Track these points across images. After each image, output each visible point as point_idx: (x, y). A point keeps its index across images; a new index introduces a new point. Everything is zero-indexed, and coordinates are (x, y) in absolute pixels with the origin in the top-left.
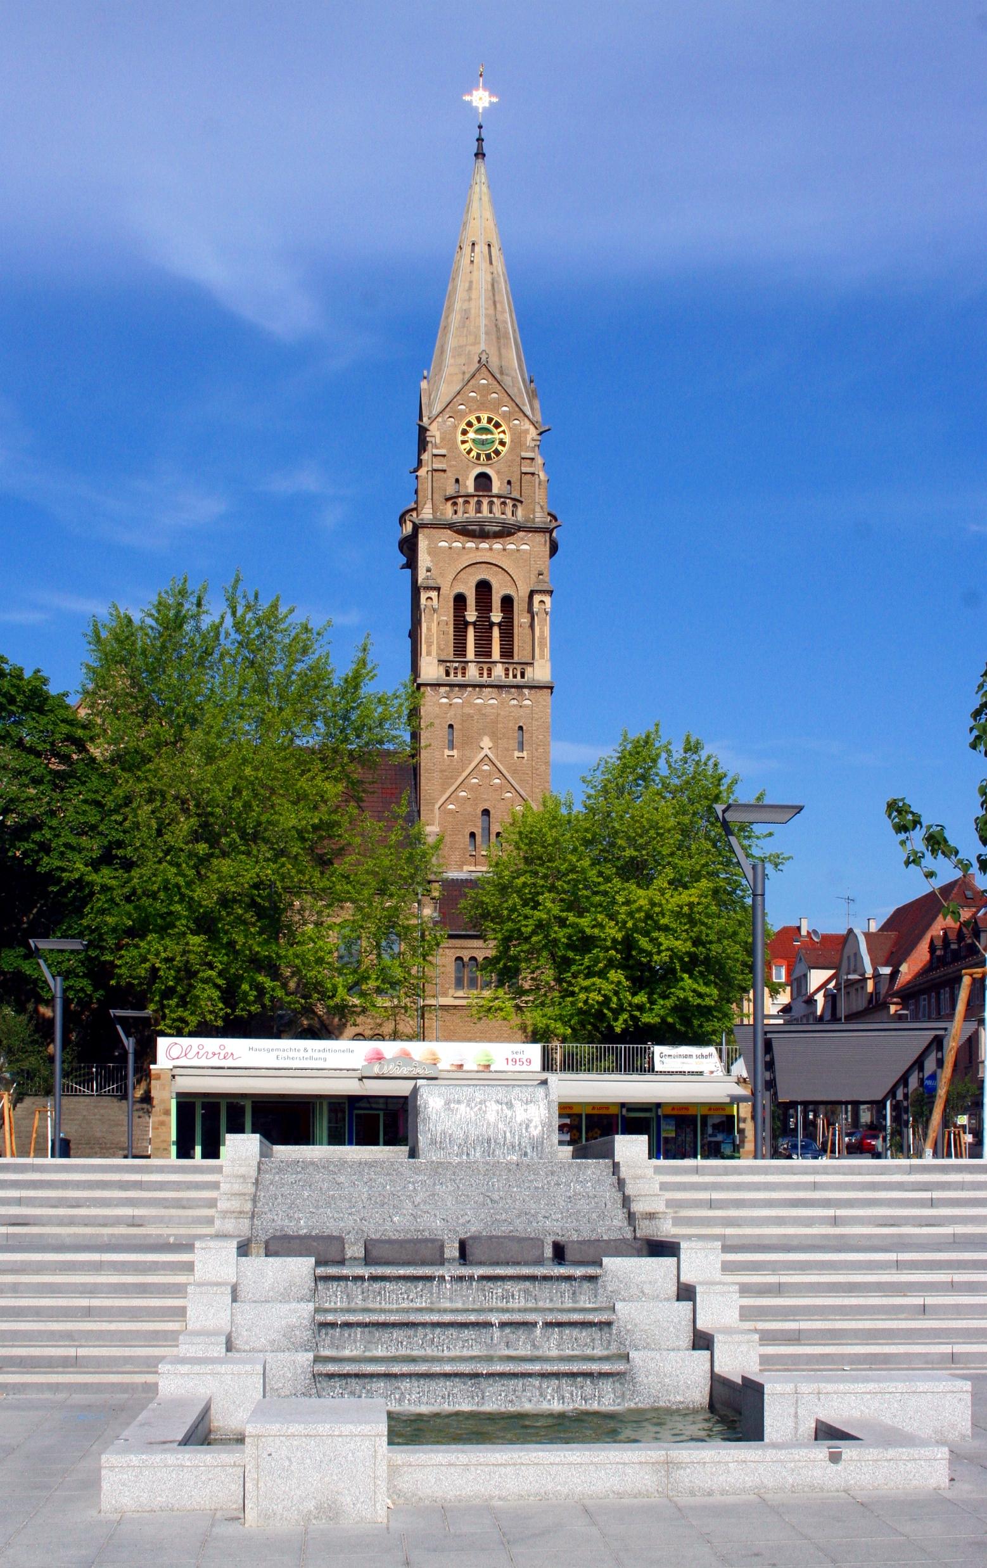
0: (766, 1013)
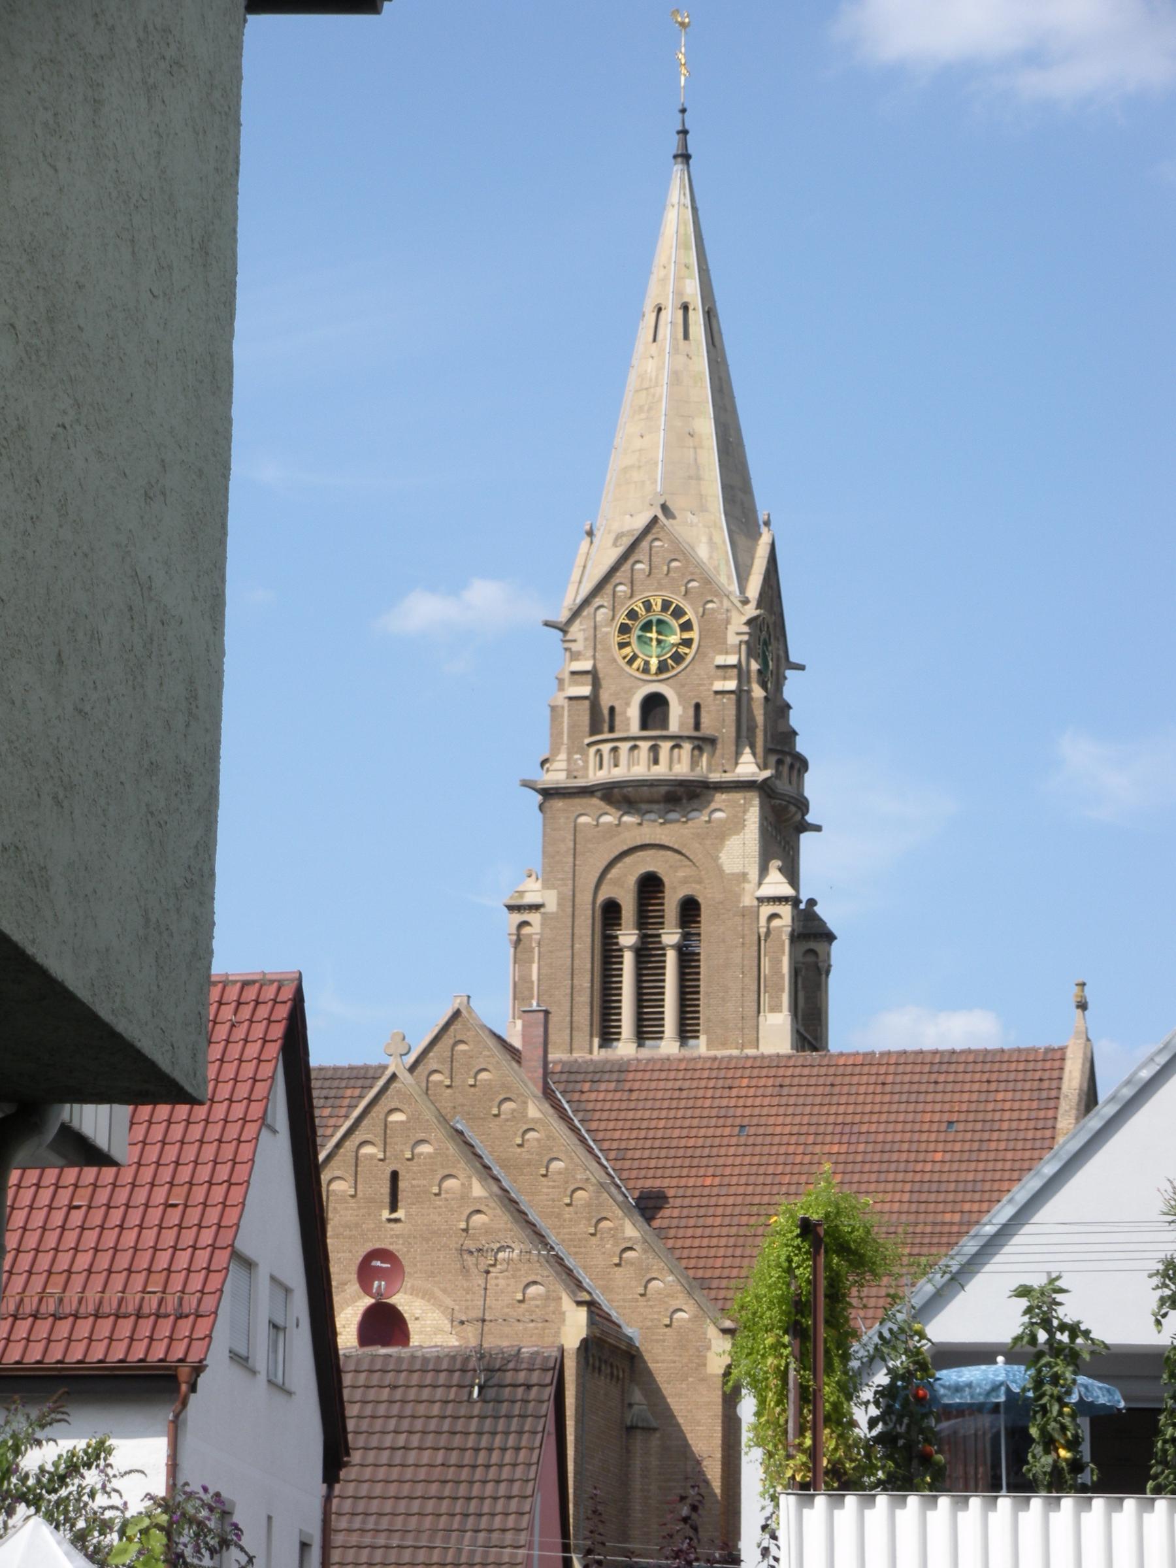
0: (733, 697)
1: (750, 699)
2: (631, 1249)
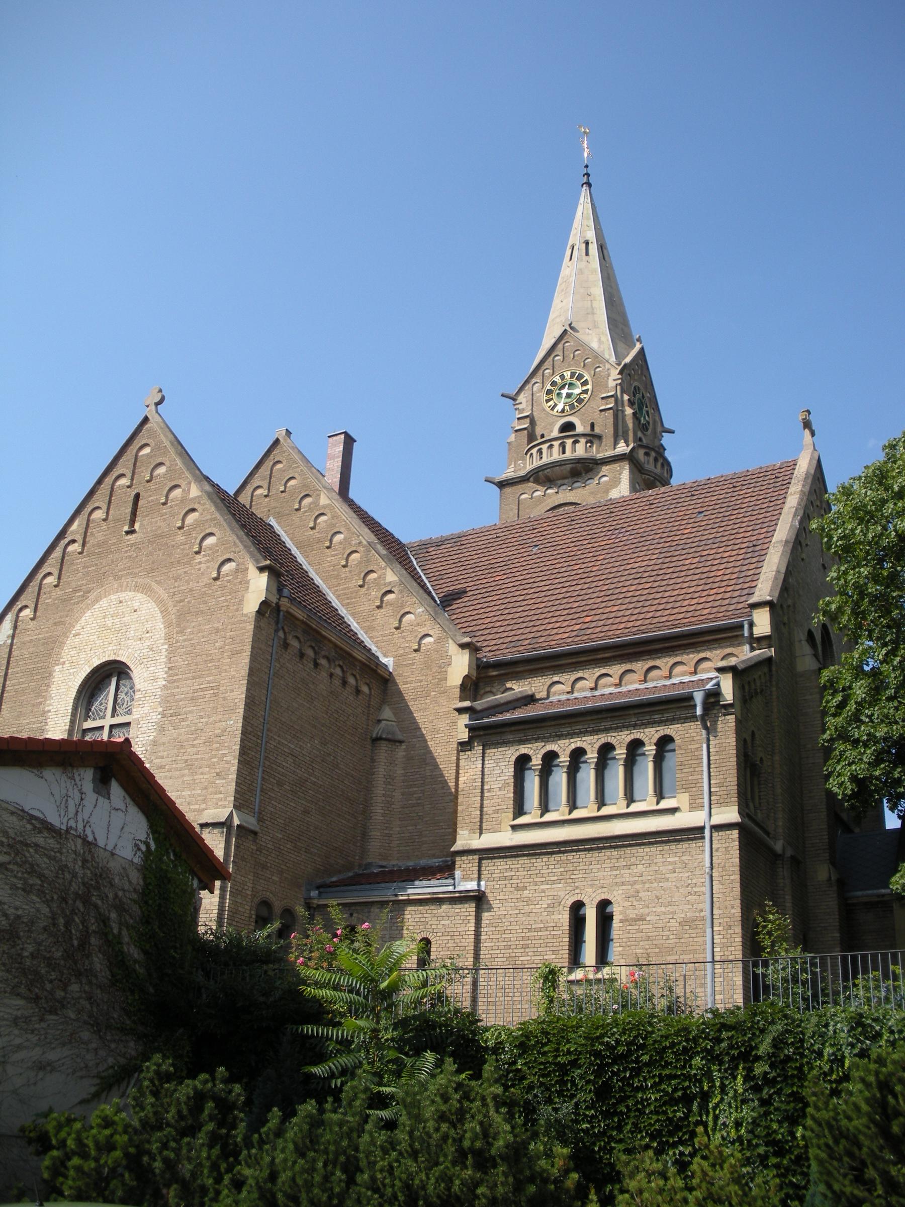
1: (624, 416)
2: (390, 592)
